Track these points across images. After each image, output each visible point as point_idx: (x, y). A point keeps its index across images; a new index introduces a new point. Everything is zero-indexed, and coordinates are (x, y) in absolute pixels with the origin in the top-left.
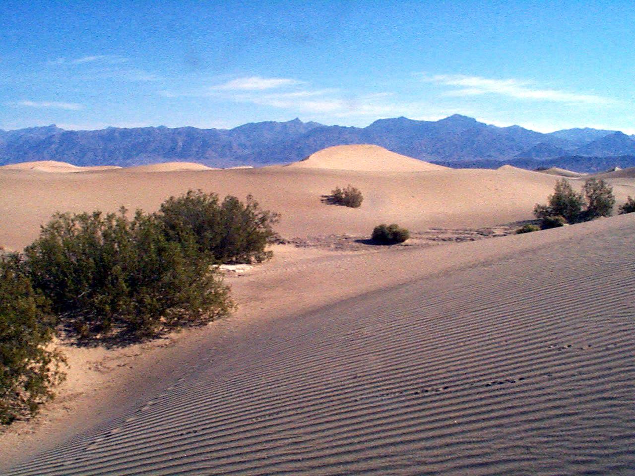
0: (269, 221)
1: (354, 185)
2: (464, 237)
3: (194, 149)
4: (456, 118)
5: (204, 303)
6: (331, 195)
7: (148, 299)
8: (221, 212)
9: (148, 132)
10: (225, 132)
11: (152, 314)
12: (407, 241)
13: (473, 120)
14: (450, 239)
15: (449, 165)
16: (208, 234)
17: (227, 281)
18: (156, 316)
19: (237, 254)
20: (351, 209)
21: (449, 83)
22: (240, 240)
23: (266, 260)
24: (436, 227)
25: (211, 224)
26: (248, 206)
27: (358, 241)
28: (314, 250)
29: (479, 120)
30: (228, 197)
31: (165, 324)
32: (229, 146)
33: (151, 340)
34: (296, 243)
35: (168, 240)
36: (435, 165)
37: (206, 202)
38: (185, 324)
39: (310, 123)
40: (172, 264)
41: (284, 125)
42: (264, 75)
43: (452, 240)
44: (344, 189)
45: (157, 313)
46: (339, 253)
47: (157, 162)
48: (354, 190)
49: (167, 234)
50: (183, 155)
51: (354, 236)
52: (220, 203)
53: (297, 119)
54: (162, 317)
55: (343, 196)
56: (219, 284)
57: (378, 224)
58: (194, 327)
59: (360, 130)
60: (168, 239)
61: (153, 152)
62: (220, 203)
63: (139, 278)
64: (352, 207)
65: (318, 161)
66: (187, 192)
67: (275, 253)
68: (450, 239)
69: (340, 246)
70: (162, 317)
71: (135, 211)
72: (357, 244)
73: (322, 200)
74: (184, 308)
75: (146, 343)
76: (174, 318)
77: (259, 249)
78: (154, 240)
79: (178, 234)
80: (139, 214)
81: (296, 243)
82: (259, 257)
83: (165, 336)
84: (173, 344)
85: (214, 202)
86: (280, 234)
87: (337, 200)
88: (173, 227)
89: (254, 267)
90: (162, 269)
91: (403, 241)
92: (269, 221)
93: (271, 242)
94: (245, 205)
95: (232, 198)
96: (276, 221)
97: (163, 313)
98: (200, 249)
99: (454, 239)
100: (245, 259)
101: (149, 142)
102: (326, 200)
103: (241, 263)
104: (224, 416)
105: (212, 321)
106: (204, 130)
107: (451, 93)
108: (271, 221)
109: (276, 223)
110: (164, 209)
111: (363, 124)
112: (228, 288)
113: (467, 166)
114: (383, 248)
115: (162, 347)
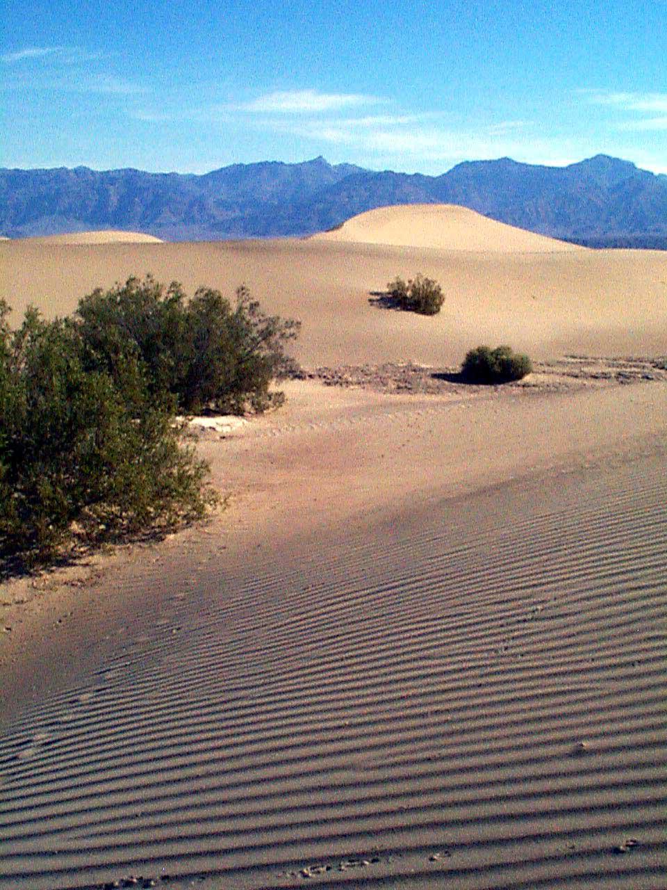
0: (278, 336)
1: (430, 274)
2: (630, 372)
3: (140, 209)
4: (600, 161)
5: (158, 495)
6: (387, 290)
7: (45, 488)
8: (187, 319)
9: (59, 176)
10: (193, 178)
11: (54, 516)
12: (528, 378)
13: (631, 166)
14: (605, 376)
15: (585, 243)
16: (165, 357)
17: (203, 449)
18: (62, 522)
19: (218, 396)
20: (428, 318)
21: (632, 107)
22: (224, 371)
23: (271, 409)
24: (577, 352)
25: (169, 339)
26: (240, 309)
27: (435, 376)
28: (357, 390)
29: (642, 165)
30: (202, 291)
31: (79, 536)
32: (200, 203)
33: (54, 568)
34: (325, 377)
35: (87, 369)
36: (561, 242)
37: (162, 299)
38: (120, 536)
39: (343, 167)
40: (95, 417)
41: (297, 169)
42: (326, 90)
43: (609, 378)
44: (410, 282)
45: (63, 517)
46: (404, 397)
47: (78, 230)
48: (428, 283)
49: (85, 356)
50: (119, 220)
51: (428, 366)
52: (185, 303)
53: (320, 157)
54: (74, 522)
55: (409, 294)
56: (188, 458)
57: (474, 347)
58: (138, 544)
59: (431, 180)
60: (90, 367)
61: (64, 213)
62: (185, 303)
63: (28, 444)
64: (424, 313)
65: (356, 230)
66: (126, 279)
67: (288, 396)
68: (605, 376)
69: (405, 384)
70: (74, 522)
71: (25, 310)
72: (437, 382)
73: (370, 300)
74: (119, 505)
75: (41, 575)
76: (99, 524)
77: (260, 388)
78: (59, 369)
79: (108, 357)
80: (31, 316)
81: (325, 377)
82: (259, 404)
83: (83, 561)
84: (95, 579)
85: (176, 300)
86: (298, 360)
87: (398, 300)
88: (98, 345)
89: (249, 421)
90: (73, 427)
91: (520, 377)
92: (278, 336)
93: (282, 376)
94: (234, 307)
95: (210, 293)
96: (292, 335)
97: (75, 514)
98: (150, 387)
99: (613, 375)
100: (232, 405)
101: (58, 194)
102: (378, 300)
103: (224, 414)
104: (105, 736)
105: (175, 532)
106: (156, 175)
107: (643, 125)
108: (282, 335)
109: (291, 339)
110: (82, 312)
111: (435, 170)
112: (205, 466)
113: (616, 244)
114: (485, 391)
115: (73, 585)
